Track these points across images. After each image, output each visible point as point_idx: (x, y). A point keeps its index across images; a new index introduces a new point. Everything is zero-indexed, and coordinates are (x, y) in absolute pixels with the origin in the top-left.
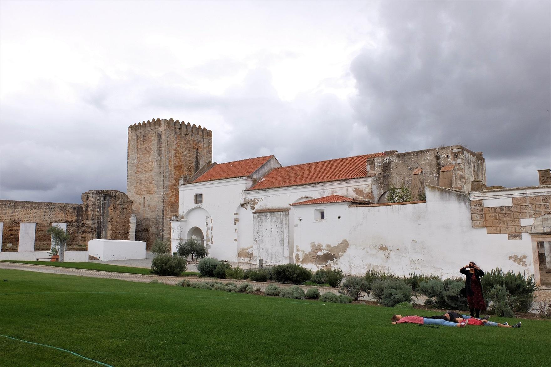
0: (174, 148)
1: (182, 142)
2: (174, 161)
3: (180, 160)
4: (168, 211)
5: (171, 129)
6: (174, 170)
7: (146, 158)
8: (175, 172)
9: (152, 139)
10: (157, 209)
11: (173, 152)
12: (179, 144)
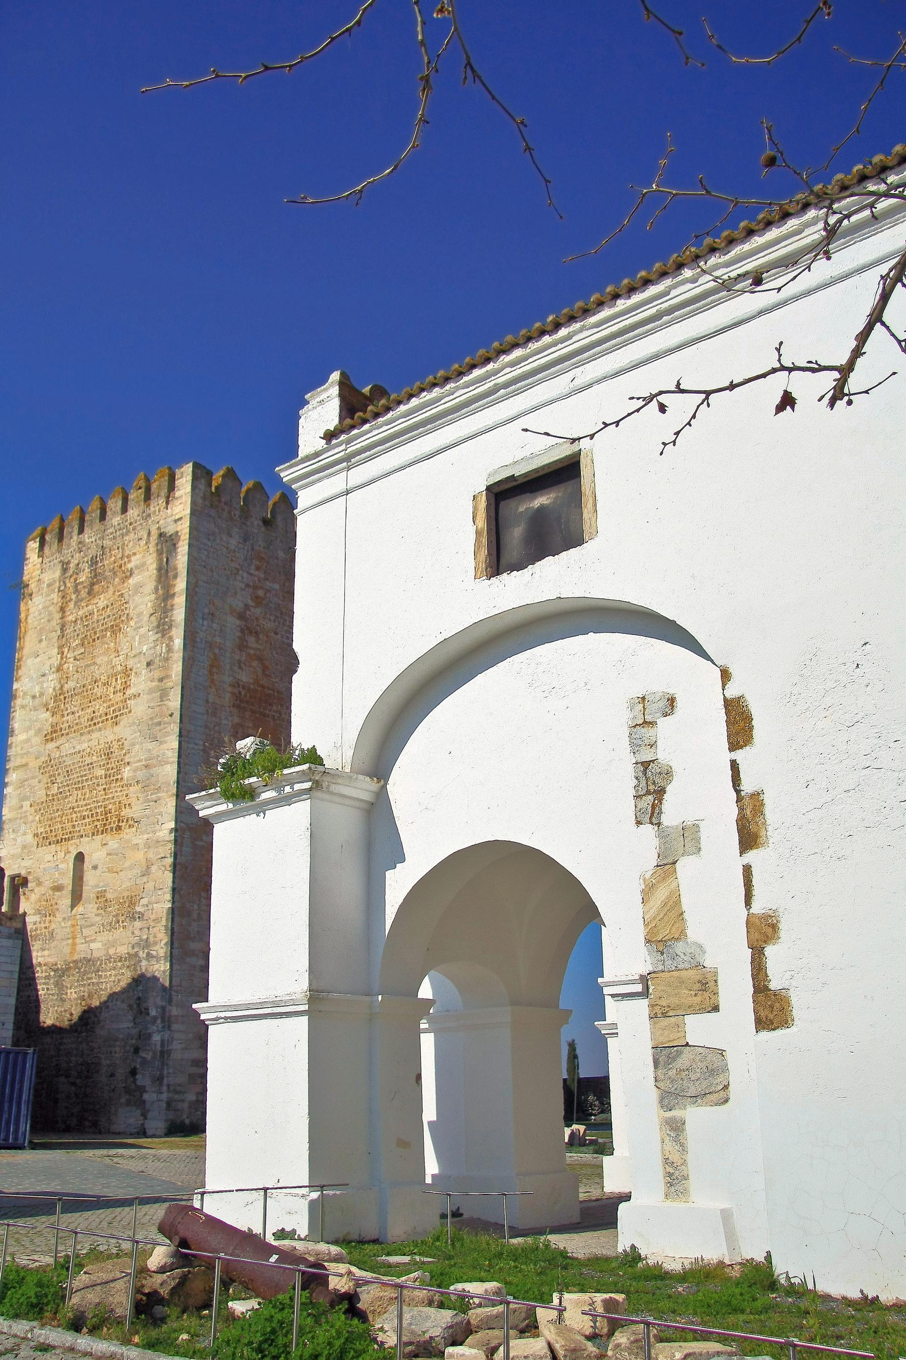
0: (239, 605)
1: (277, 586)
2: (236, 668)
3: (265, 668)
4: (195, 915)
5: (225, 515)
6: (235, 711)
7: (98, 661)
8: (236, 720)
9: (129, 566)
10: (138, 909)
11: (232, 622)
12: (260, 593)
